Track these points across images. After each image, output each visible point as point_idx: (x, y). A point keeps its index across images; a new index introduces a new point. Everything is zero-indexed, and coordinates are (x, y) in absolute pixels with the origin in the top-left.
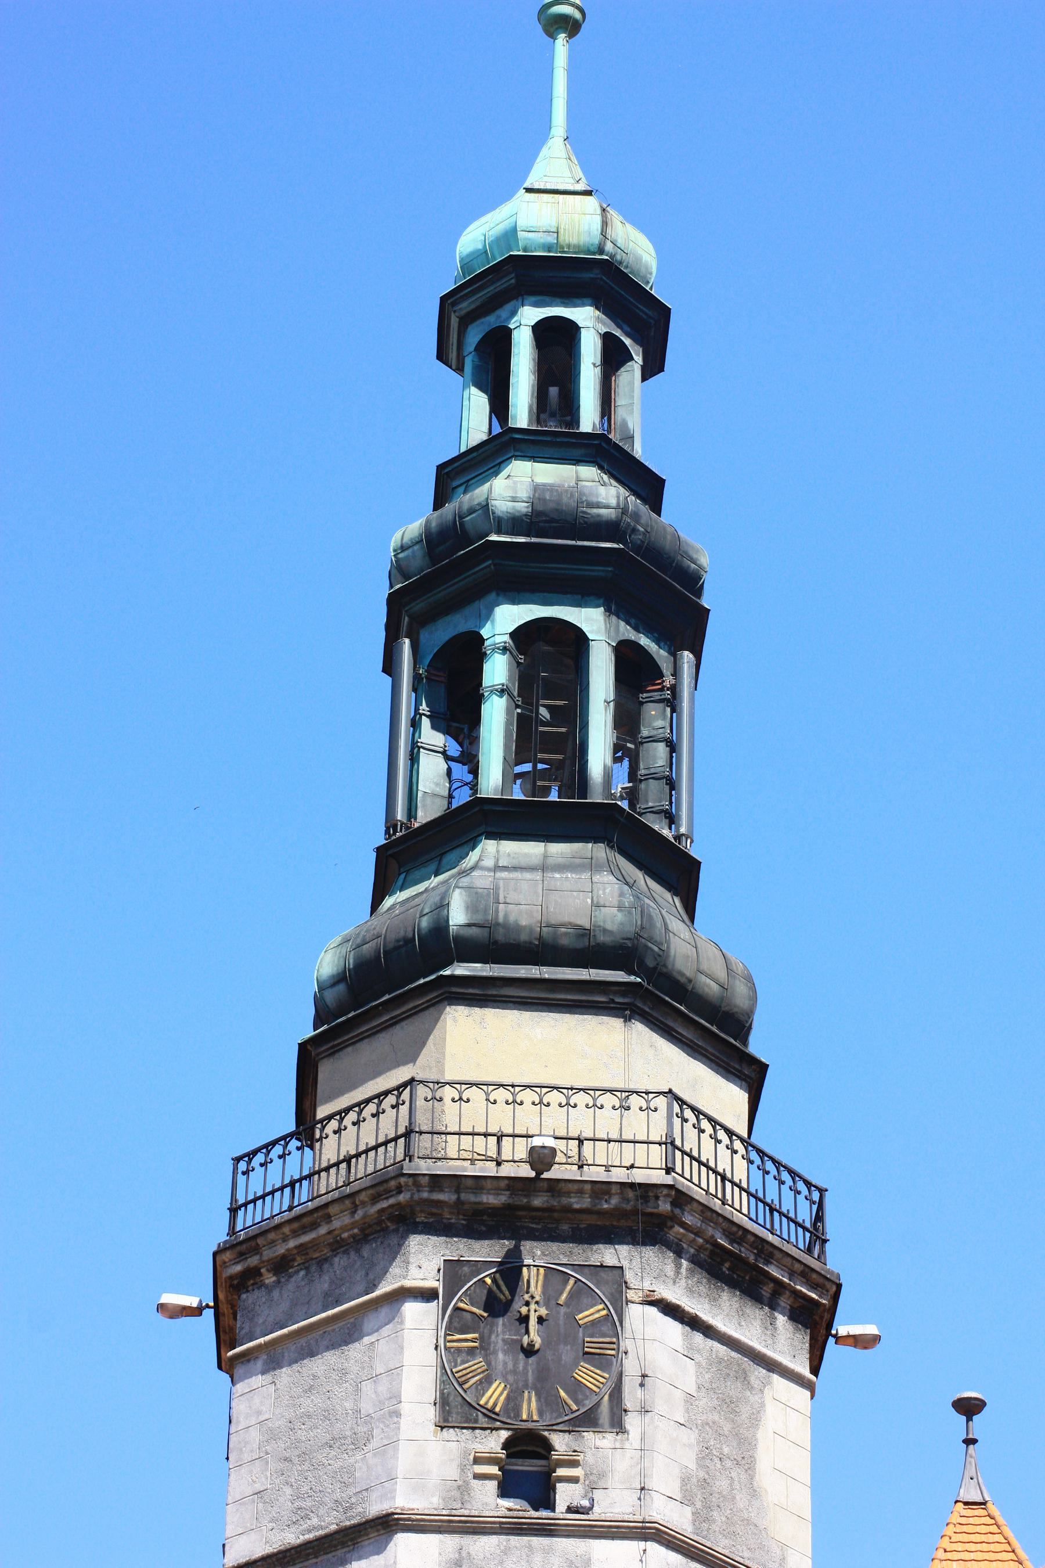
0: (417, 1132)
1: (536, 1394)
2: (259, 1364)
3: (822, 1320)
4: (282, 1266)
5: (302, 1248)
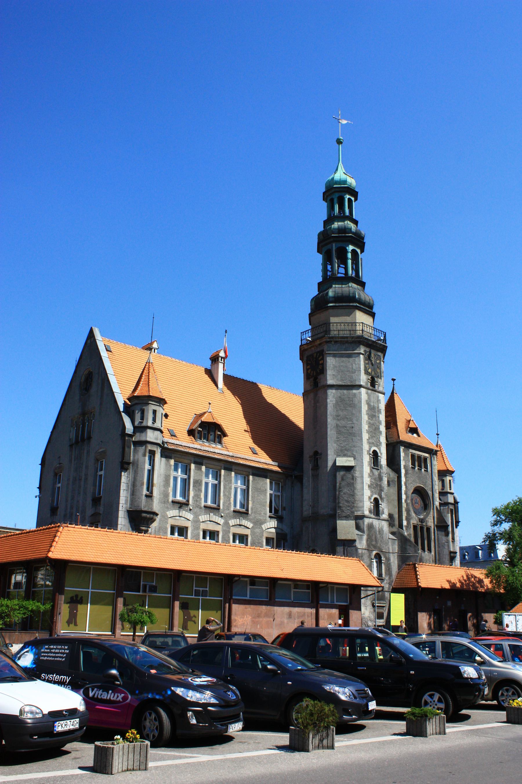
0: (363, 333)
1: (84, 437)
2: (332, 355)
3: (402, 529)
4: (336, 342)
5: (341, 341)
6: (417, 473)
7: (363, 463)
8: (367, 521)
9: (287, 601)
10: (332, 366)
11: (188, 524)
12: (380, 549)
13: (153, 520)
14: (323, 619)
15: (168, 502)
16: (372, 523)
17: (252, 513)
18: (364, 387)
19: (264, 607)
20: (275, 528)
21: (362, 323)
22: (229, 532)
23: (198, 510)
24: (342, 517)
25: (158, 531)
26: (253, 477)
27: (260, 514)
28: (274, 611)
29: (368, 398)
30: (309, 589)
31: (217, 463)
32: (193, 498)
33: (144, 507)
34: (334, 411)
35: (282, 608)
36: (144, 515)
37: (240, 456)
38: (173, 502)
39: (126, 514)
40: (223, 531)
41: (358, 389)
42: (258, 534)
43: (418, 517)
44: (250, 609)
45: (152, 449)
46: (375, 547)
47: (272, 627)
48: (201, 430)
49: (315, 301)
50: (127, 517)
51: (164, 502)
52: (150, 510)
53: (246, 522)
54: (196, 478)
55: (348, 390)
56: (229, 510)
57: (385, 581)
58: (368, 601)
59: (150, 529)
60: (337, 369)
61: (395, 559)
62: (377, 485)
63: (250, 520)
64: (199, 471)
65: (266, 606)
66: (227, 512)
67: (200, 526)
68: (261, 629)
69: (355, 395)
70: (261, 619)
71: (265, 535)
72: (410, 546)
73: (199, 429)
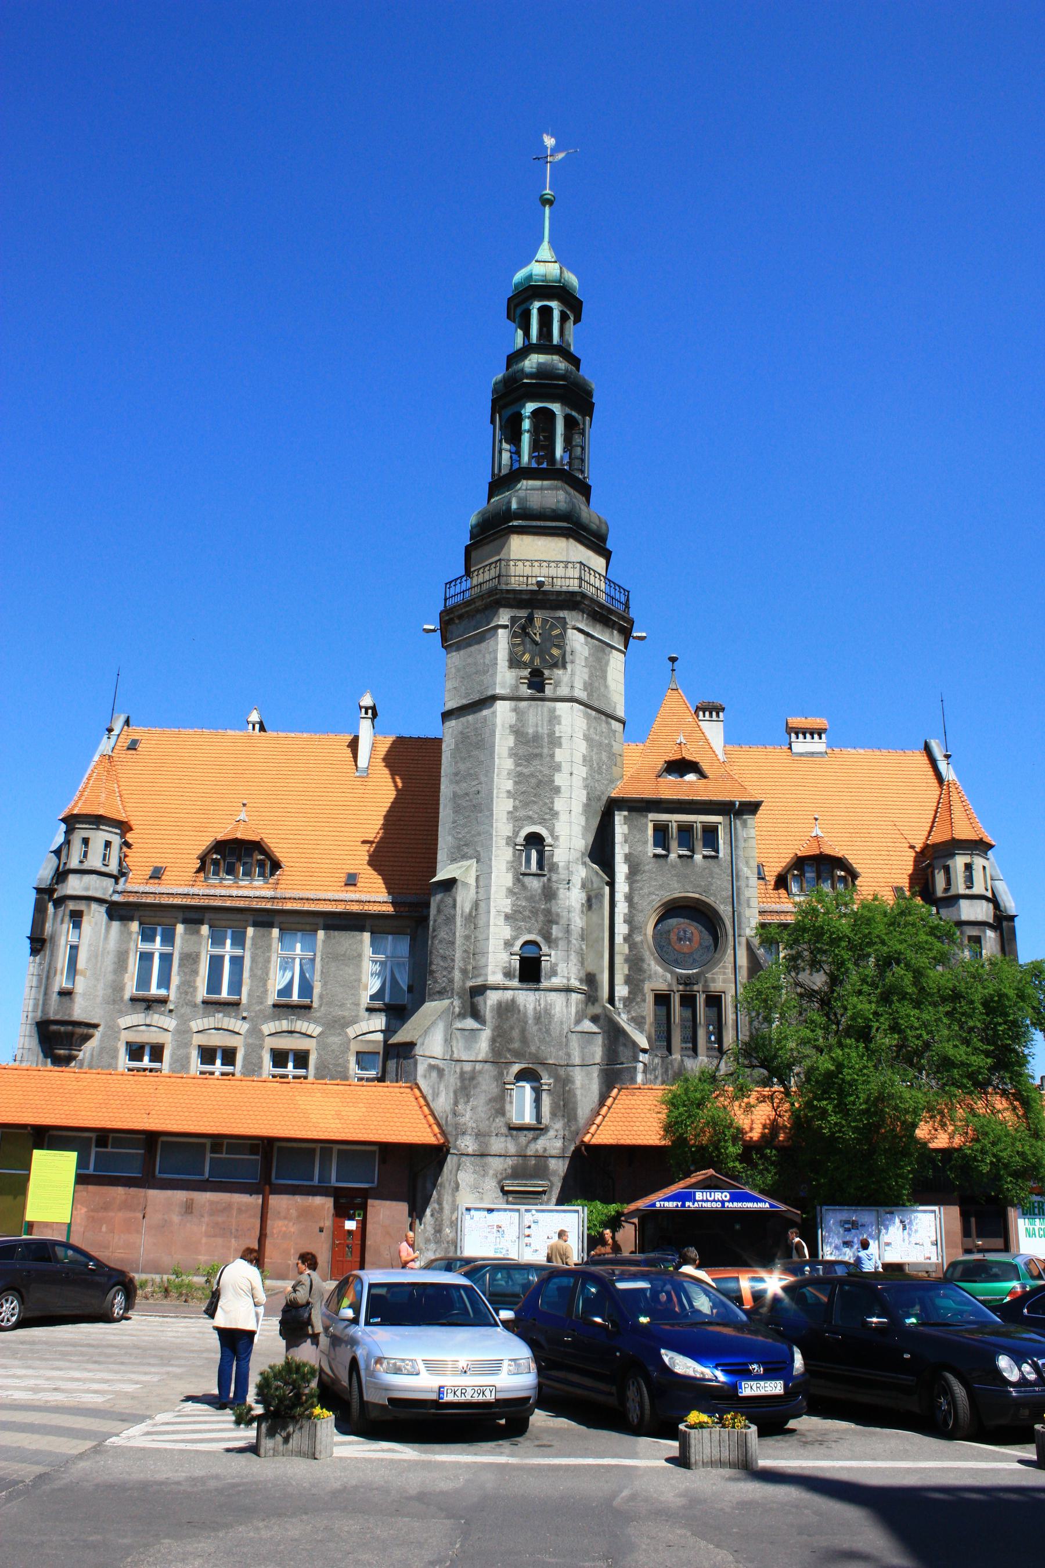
2: (454, 648)
6: (673, 866)
7: (491, 867)
8: (493, 998)
9: (197, 1177)
10: (453, 670)
11: (167, 1039)
12: (537, 1058)
13: (87, 1037)
14: (285, 1218)
15: (122, 1001)
16: (513, 1001)
17: (320, 1006)
18: (503, 698)
19: (120, 1190)
20: (381, 1031)
21: (581, 563)
22: (262, 1047)
23: (189, 1011)
24: (434, 994)
25: (99, 1055)
26: (326, 934)
27: (342, 1005)
28: (146, 1197)
29: (518, 719)
30: (256, 1154)
31: (239, 916)
32: (178, 987)
33: (55, 1014)
34: (451, 765)
35: (169, 1193)
36: (54, 1028)
37: (293, 896)
38: (133, 1000)
39: (34, 1029)
40: (247, 1046)
41: (491, 706)
42: (334, 1047)
43: (672, 973)
44: (85, 1194)
45: (77, 908)
46: (519, 1055)
47: (139, 1232)
48: (219, 857)
49: (499, 553)
50: (36, 1036)
51: (114, 1001)
52: (66, 1018)
53: (306, 1024)
54: (186, 950)
55: (475, 712)
56: (261, 1003)
57: (551, 1133)
58: (487, 1179)
59: (81, 1054)
60: (461, 673)
61: (591, 1079)
62: (535, 912)
63: (316, 1021)
64: (194, 938)
65: (127, 1188)
66: (258, 1008)
67: (191, 1041)
68: (111, 1235)
69: (485, 718)
70: (111, 1214)
71: (354, 1047)
72: (625, 1045)
73: (214, 856)
